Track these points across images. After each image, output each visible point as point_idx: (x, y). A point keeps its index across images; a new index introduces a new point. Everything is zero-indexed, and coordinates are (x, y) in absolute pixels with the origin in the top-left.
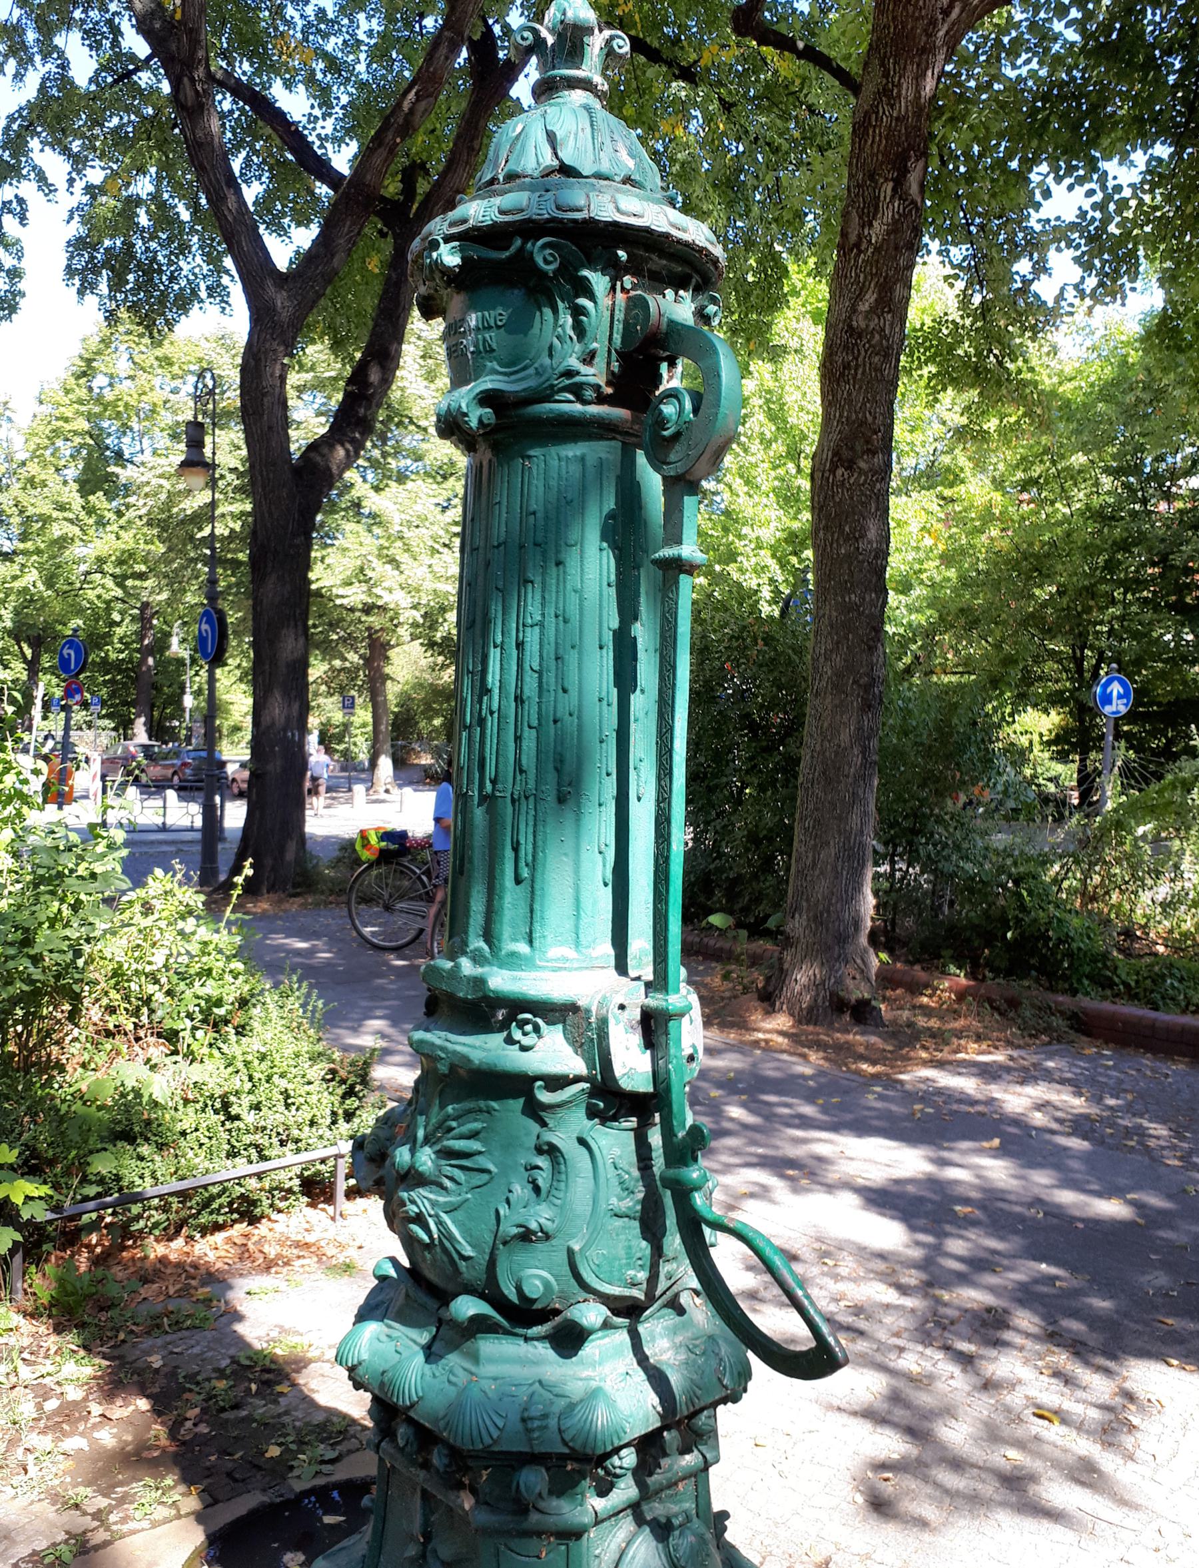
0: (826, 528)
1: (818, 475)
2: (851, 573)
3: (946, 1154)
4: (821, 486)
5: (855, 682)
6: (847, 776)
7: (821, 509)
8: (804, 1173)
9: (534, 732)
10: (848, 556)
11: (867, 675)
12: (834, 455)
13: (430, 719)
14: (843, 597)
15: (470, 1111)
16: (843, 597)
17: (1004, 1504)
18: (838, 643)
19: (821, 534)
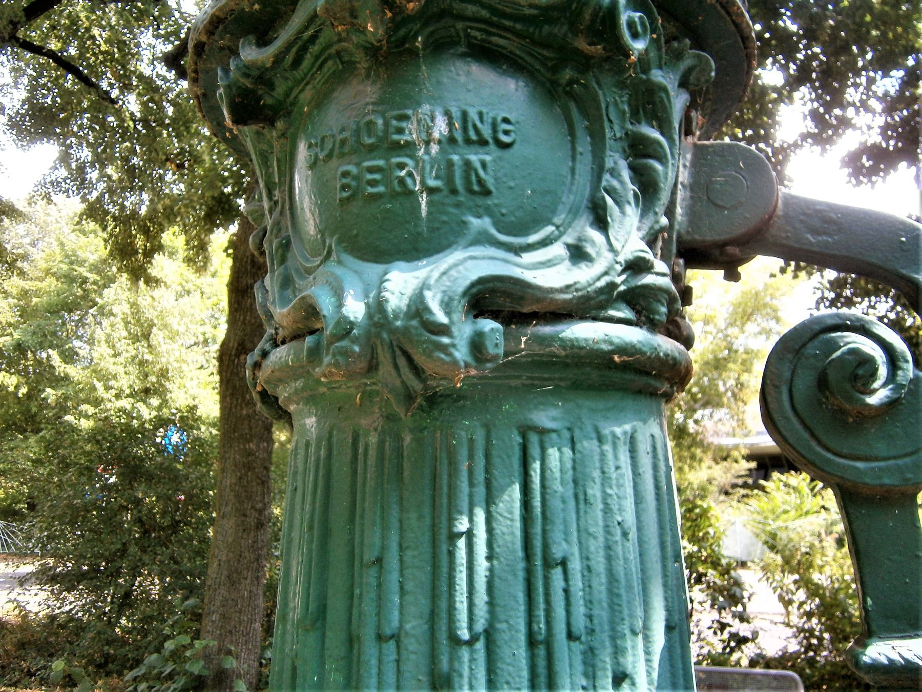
0: (232, 395)
1: (225, 358)
2: (251, 429)
3: (263, 317)
4: (228, 366)
5: (253, 507)
6: (246, 578)
7: (228, 381)
8: (874, 391)
9: (558, 552)
10: (248, 416)
11: (261, 501)
12: (239, 345)
13: (828, 9)
14: (244, 446)
15: (607, 115)
16: (244, 446)
17: (367, 305)
18: (240, 478)
19: (228, 399)
